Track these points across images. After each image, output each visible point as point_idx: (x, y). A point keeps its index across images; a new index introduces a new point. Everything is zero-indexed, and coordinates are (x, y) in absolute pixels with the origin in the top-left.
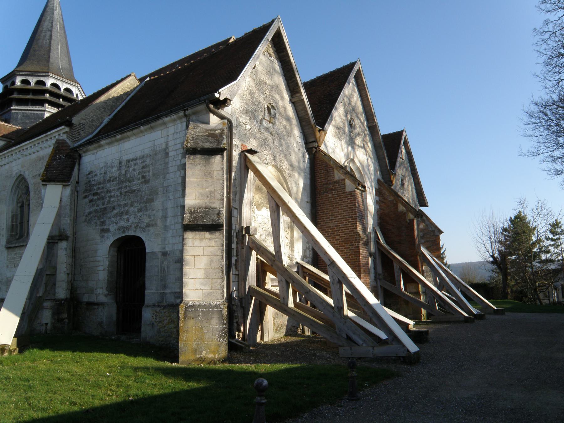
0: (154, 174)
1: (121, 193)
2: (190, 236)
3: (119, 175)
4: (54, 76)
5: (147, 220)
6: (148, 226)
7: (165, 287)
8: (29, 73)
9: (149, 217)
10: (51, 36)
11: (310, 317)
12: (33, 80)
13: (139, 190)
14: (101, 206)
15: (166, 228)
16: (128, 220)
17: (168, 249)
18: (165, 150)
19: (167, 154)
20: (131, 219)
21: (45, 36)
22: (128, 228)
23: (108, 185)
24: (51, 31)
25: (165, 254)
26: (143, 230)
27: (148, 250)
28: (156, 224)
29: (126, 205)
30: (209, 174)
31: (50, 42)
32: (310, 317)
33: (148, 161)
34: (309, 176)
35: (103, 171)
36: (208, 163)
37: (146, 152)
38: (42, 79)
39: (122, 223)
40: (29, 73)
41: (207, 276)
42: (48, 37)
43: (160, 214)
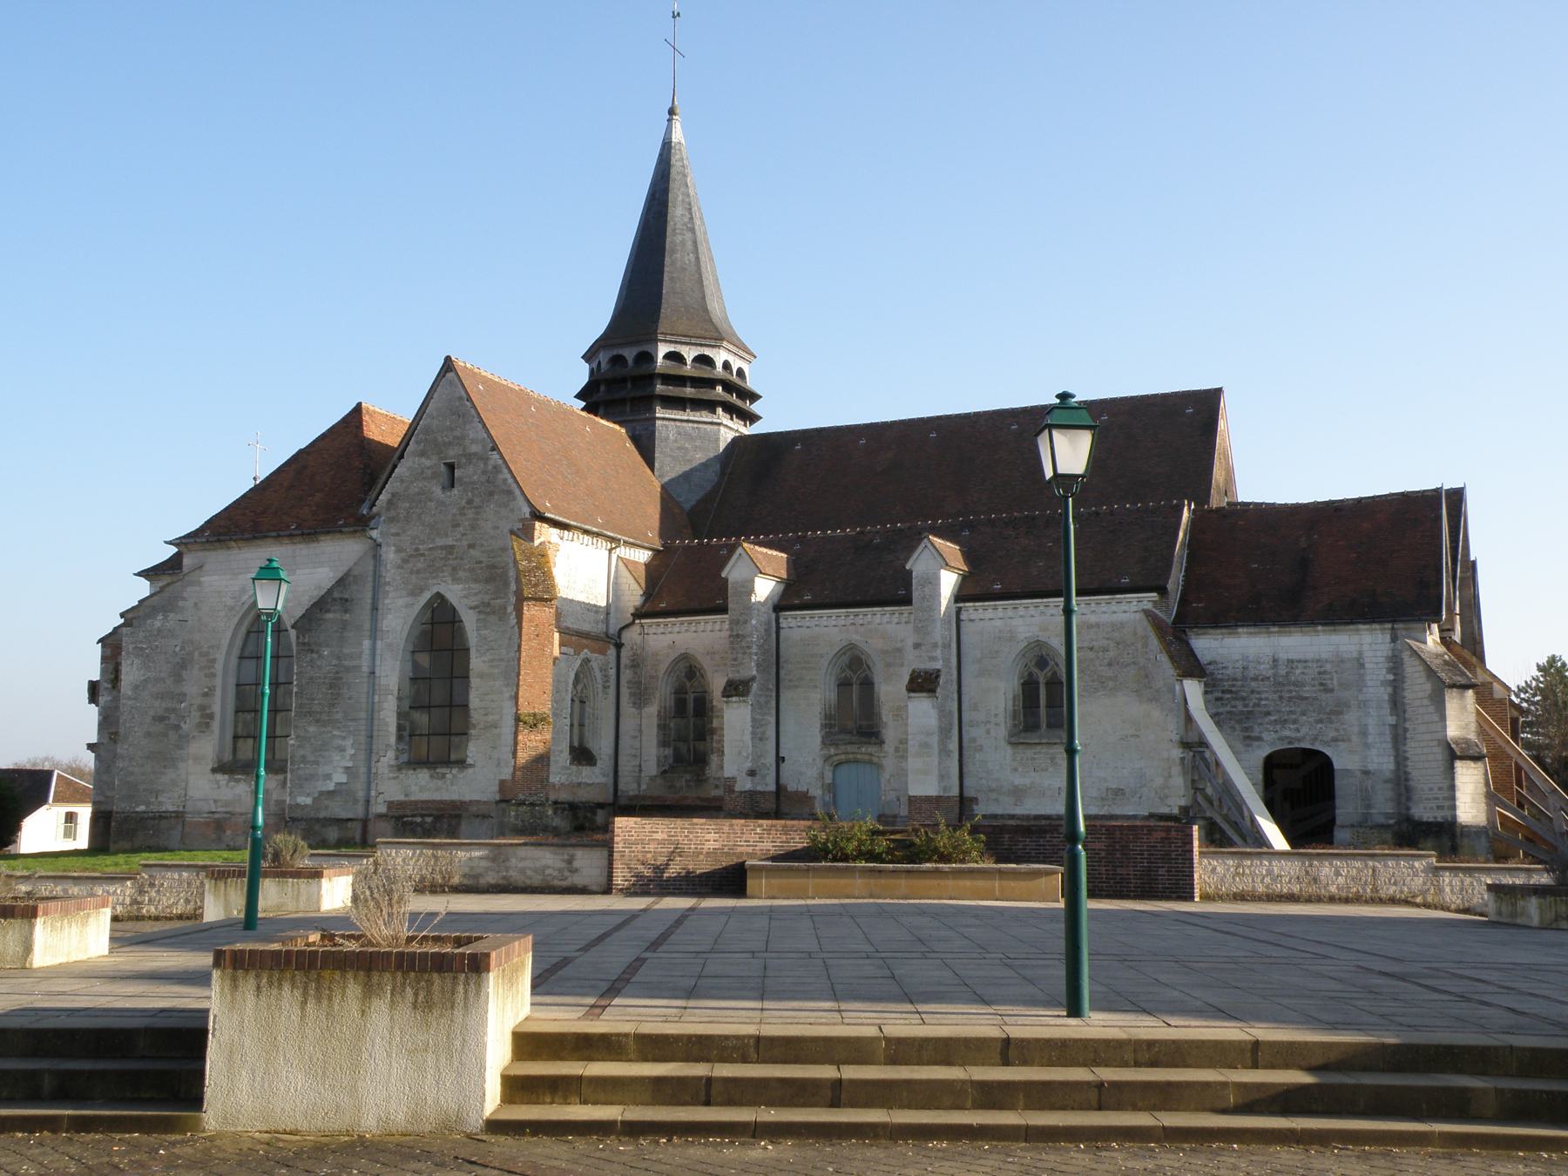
0: (1340, 684)
1: (1281, 698)
2: (1458, 764)
3: (1275, 675)
4: (731, 347)
5: (1332, 734)
6: (1335, 740)
7: (1369, 806)
8: (684, 339)
9: (1337, 730)
10: (695, 242)
11: (828, 901)
12: (689, 353)
13: (1315, 699)
14: (1240, 708)
15: (1367, 746)
16: (1298, 730)
17: (1371, 767)
18: (1358, 659)
19: (1362, 666)
20: (1304, 730)
21: (683, 243)
22: (1299, 740)
23: (1253, 684)
24: (693, 230)
25: (1366, 773)
26: (1327, 744)
27: (1336, 766)
28: (1349, 740)
29: (1291, 712)
30: (1464, 708)
31: (697, 258)
32: (828, 901)
33: (1328, 667)
34: (1252, 630)
35: (1239, 665)
36: (1462, 697)
37: (1324, 656)
38: (707, 352)
39: (1287, 733)
40: (684, 339)
41: (1474, 801)
42: (689, 244)
43: (1356, 729)
